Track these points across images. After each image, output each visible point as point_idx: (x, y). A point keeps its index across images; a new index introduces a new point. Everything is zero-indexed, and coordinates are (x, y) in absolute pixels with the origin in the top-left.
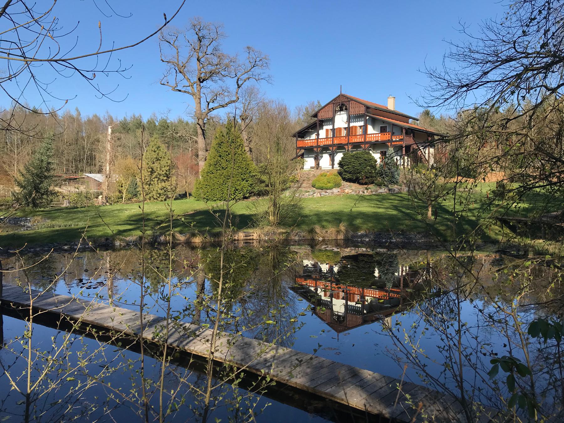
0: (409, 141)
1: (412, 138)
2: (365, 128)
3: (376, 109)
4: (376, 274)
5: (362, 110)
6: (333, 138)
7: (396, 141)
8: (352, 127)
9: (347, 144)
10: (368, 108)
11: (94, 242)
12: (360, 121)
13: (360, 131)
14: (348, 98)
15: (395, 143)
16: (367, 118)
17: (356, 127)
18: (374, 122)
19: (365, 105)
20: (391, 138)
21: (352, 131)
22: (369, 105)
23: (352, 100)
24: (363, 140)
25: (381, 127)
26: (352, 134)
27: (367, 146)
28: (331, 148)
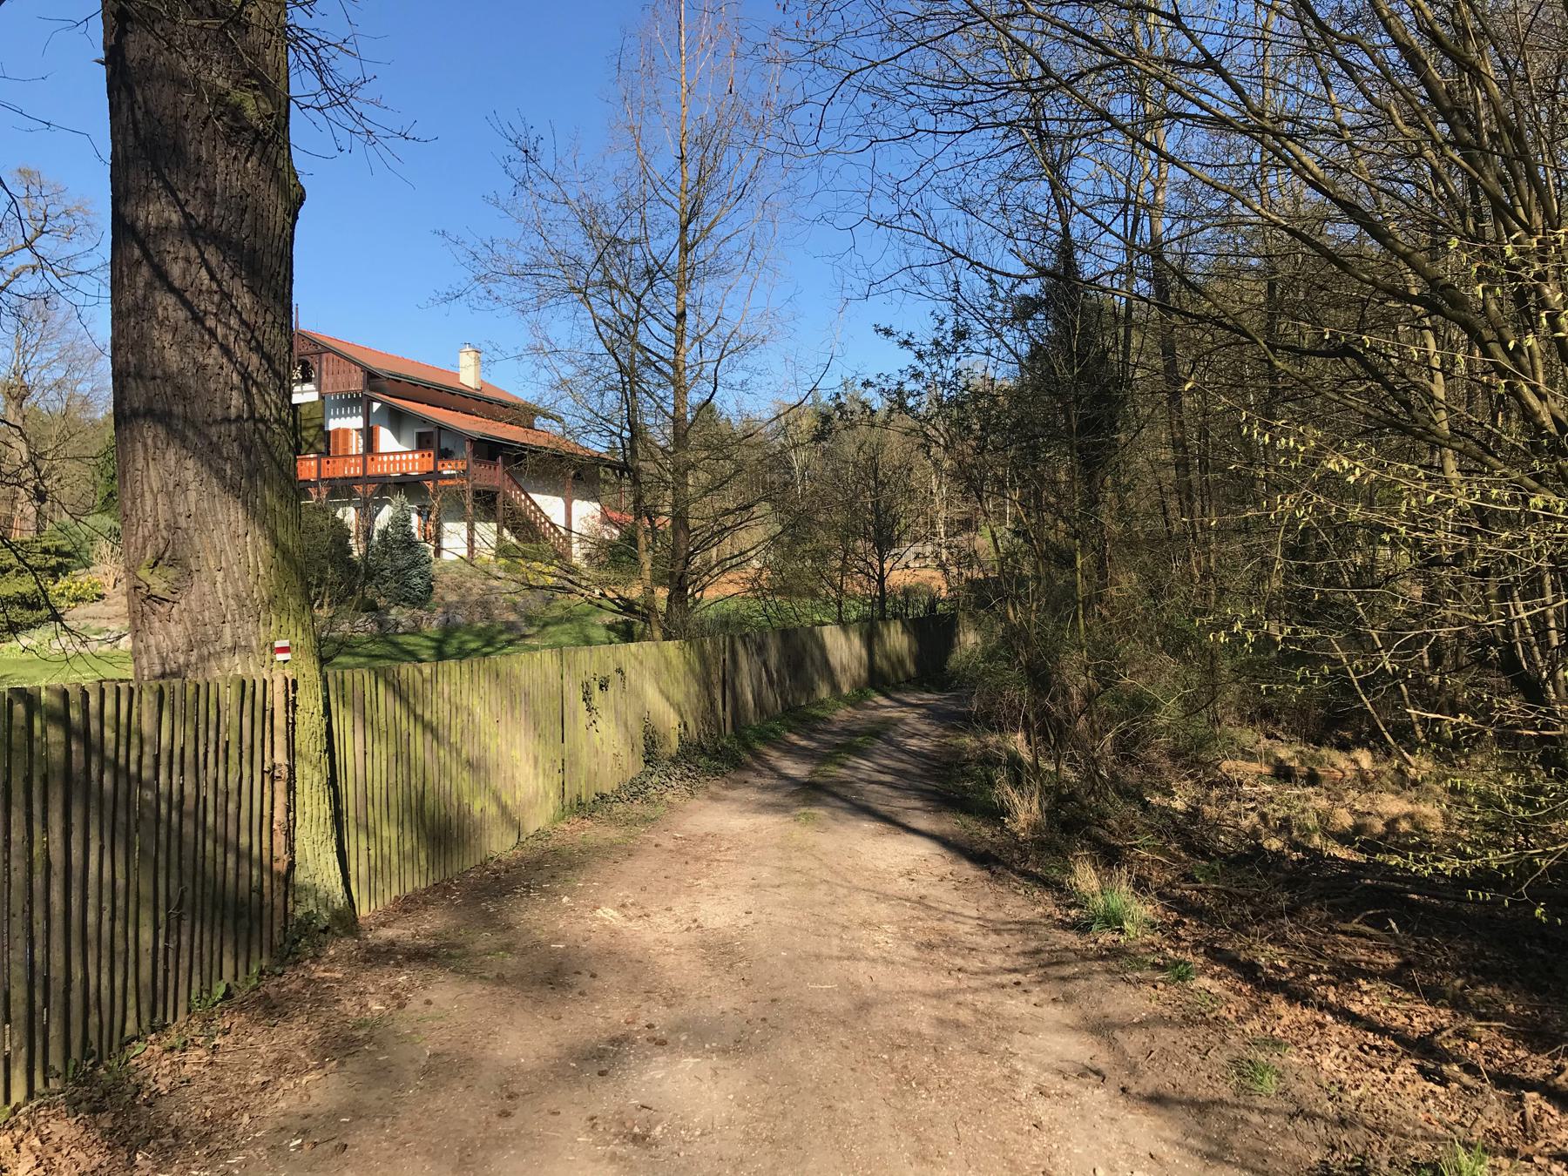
0: (492, 476)
1: (500, 469)
2: (369, 436)
3: (397, 379)
4: (1538, 911)
5: (356, 382)
6: (364, 455)
7: (451, 477)
8: (336, 431)
9: (315, 484)
10: (371, 377)
11: (576, 1060)
12: (351, 415)
13: (356, 445)
14: (316, 344)
15: (447, 482)
16: (376, 406)
17: (346, 431)
18: (397, 420)
19: (364, 369)
20: (436, 466)
21: (336, 444)
22: (375, 364)
23: (328, 350)
24: (359, 472)
25: (420, 435)
26: (336, 451)
27: (371, 488)
28: (359, 489)
